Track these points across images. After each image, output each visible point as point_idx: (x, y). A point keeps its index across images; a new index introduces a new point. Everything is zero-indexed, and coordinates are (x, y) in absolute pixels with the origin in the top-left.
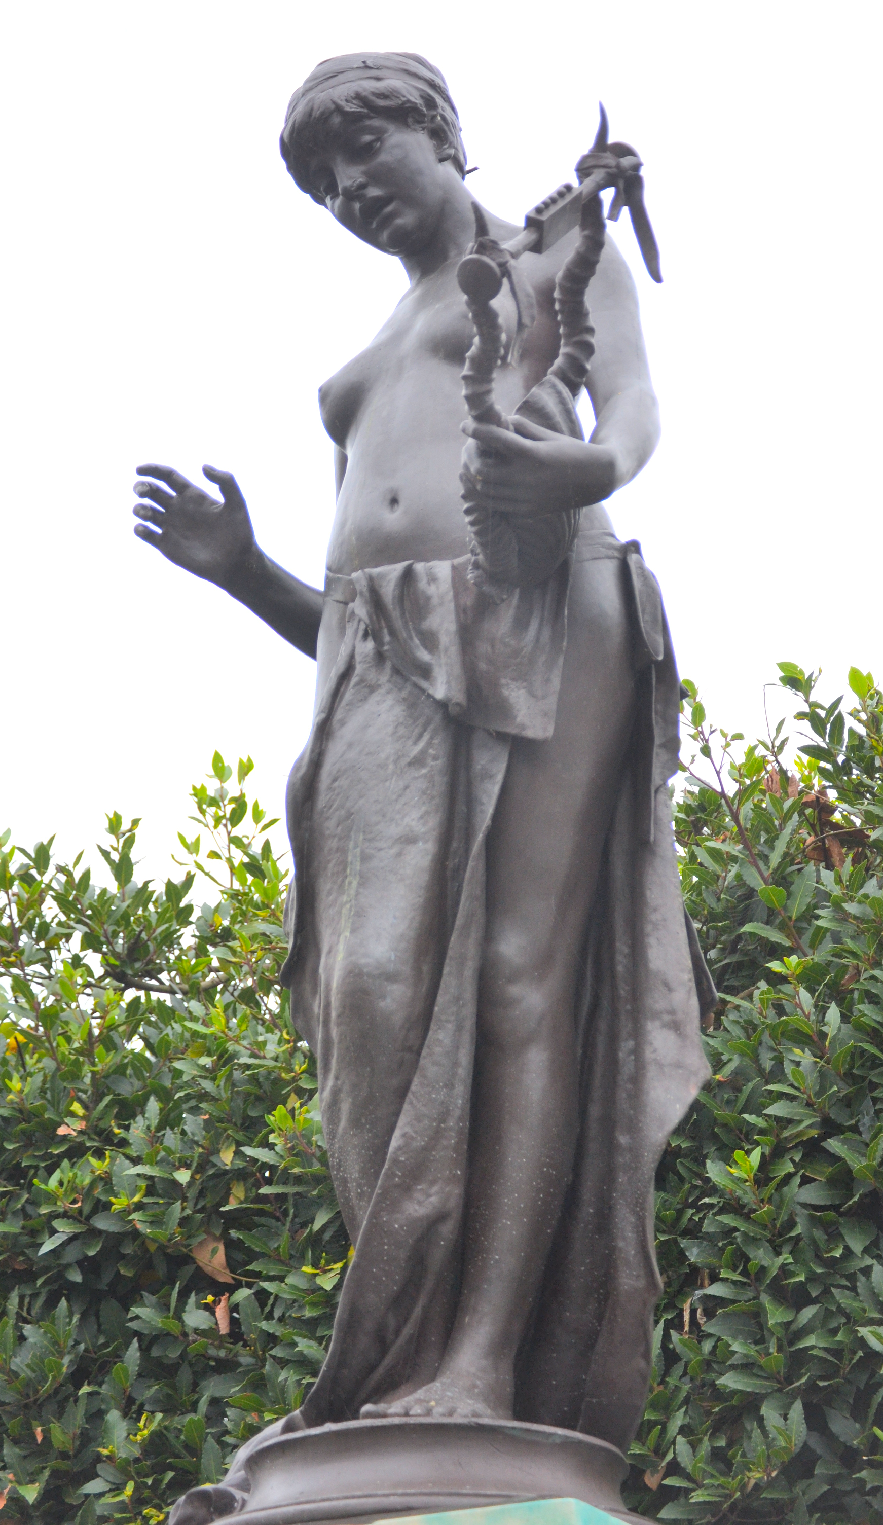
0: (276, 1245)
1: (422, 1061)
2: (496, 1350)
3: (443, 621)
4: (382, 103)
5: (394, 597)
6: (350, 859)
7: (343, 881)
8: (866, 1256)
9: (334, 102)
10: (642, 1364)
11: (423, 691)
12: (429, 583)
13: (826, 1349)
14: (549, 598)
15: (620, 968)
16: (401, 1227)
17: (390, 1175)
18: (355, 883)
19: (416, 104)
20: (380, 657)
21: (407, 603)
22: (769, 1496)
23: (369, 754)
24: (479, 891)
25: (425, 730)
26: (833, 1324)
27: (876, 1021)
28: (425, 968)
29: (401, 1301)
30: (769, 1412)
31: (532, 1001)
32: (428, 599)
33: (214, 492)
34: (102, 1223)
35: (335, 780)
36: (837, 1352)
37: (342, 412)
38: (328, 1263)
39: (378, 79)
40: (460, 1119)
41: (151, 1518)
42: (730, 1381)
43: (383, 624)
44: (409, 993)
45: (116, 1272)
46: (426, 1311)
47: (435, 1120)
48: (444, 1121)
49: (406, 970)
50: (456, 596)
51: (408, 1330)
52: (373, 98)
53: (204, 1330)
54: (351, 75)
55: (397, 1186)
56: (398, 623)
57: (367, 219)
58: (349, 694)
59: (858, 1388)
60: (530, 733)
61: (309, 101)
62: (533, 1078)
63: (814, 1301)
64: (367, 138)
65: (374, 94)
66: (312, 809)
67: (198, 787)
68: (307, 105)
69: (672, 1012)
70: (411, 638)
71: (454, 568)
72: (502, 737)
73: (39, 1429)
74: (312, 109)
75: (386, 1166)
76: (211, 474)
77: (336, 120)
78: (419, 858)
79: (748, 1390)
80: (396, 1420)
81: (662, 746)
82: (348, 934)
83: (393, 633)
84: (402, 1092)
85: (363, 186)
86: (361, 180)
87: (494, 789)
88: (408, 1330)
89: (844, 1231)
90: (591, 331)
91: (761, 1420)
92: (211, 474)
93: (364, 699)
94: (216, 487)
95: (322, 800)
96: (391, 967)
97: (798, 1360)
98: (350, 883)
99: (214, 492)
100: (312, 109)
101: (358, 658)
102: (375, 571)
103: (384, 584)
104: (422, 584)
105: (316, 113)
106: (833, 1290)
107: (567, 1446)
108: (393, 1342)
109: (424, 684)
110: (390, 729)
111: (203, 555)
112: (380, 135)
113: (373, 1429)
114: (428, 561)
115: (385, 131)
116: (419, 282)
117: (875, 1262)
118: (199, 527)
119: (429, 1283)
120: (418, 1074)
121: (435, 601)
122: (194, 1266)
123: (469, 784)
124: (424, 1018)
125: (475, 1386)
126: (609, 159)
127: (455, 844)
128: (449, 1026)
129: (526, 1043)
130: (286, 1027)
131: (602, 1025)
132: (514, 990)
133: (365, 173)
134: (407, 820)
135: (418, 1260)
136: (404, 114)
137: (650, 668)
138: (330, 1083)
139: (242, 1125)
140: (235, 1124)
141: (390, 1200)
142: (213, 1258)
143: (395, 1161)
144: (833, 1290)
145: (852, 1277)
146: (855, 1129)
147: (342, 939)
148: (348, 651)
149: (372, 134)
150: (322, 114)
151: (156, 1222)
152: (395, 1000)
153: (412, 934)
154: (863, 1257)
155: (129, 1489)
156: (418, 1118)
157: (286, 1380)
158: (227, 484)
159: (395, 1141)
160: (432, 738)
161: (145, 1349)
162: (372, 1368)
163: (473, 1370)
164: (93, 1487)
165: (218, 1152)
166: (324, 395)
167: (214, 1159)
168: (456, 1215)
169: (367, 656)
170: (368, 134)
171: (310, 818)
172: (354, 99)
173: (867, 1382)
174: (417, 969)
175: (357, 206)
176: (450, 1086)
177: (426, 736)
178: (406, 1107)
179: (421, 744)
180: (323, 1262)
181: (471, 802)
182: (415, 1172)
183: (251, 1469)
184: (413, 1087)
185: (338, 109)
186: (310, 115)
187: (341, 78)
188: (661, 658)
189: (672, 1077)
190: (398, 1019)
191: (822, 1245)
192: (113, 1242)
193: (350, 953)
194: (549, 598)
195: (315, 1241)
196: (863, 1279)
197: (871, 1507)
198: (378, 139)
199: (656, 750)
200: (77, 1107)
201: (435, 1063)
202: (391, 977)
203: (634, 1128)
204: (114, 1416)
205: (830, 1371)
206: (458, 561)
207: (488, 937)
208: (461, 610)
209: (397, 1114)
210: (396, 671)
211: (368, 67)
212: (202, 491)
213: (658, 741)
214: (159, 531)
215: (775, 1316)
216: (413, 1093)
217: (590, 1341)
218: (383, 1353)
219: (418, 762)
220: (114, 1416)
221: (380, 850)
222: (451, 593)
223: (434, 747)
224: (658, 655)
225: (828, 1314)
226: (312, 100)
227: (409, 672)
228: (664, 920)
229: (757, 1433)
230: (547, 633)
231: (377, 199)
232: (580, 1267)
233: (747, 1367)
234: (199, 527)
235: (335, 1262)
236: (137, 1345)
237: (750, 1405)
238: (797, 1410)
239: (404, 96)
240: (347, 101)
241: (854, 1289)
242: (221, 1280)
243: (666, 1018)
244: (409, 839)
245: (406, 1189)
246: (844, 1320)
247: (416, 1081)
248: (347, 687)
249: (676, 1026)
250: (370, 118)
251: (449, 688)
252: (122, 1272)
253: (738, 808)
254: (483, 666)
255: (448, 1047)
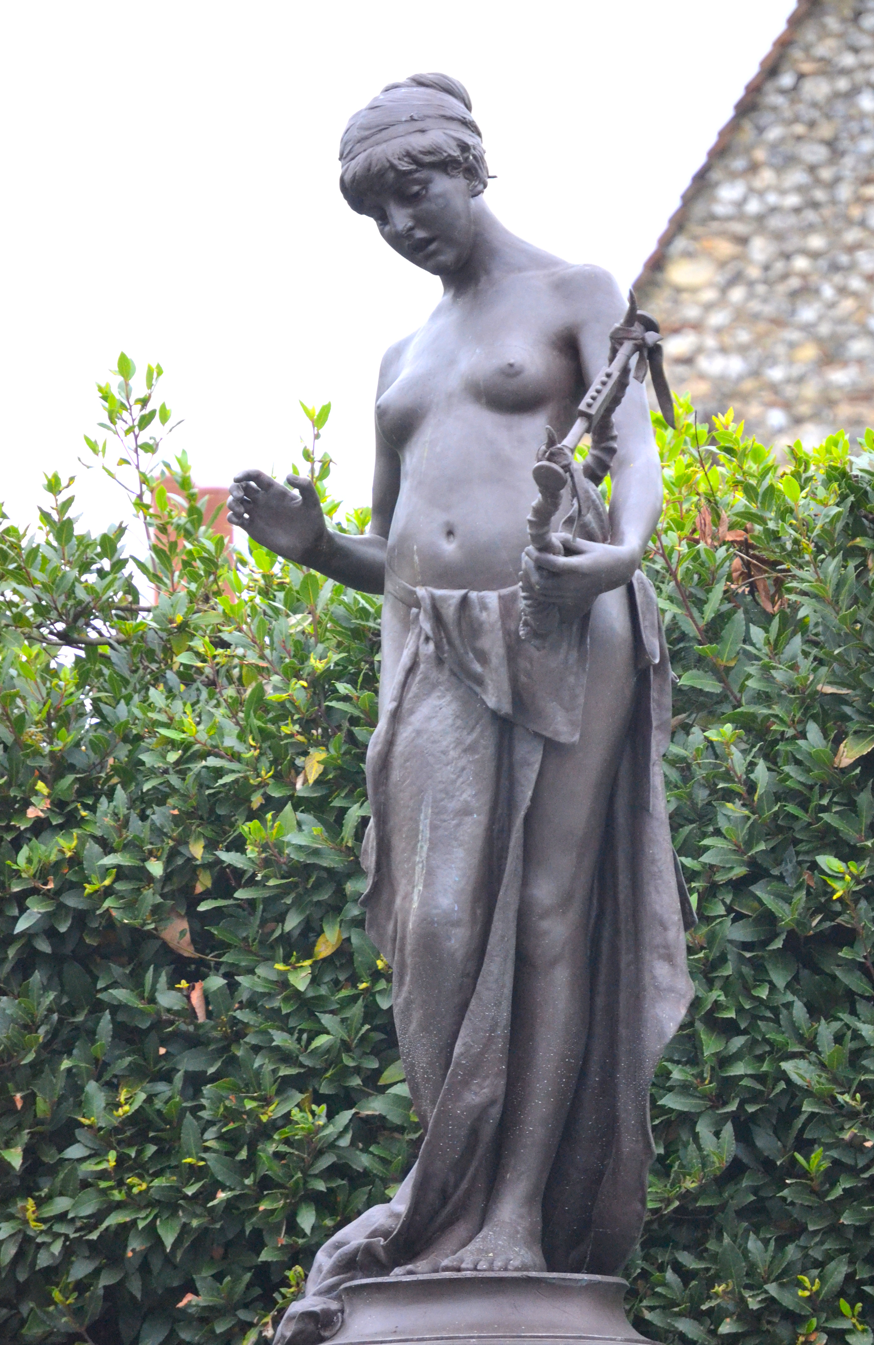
0: (244, 935)
1: (478, 988)
2: (529, 1200)
3: (494, 644)
4: (428, 159)
6: (421, 828)
7: (416, 845)
8: (788, 993)
9: (389, 161)
10: (639, 1206)
11: (477, 694)
12: (481, 611)
13: (751, 1076)
14: (575, 628)
15: (622, 897)
16: (462, 1113)
17: (455, 1074)
21: (464, 624)
22: (704, 1205)
23: (434, 742)
24: (519, 852)
25: (477, 723)
26: (758, 1052)
27: (800, 782)
28: (479, 912)
29: (460, 1168)
30: (703, 1129)
31: (557, 932)
32: (481, 624)
34: (71, 901)
35: (406, 761)
36: (760, 1078)
38: (298, 961)
39: (423, 131)
40: (505, 1028)
41: (133, 1186)
42: (670, 1101)
43: (443, 635)
45: (87, 948)
46: (477, 1170)
47: (486, 1032)
48: (494, 1031)
49: (466, 917)
52: (421, 156)
53: (178, 1011)
54: (401, 129)
56: (457, 642)
58: (414, 689)
59: (780, 1110)
60: (563, 739)
61: (367, 157)
62: (558, 994)
63: (744, 1032)
64: (416, 188)
65: (421, 152)
66: (387, 778)
67: (103, 385)
68: (366, 160)
69: (667, 947)
71: (501, 598)
72: (537, 735)
73: (18, 1096)
74: (370, 164)
75: (451, 1068)
77: (391, 175)
78: (473, 828)
79: (686, 1110)
80: (468, 1274)
81: (658, 727)
82: (421, 888)
86: (410, 224)
87: (532, 774)
88: (464, 1185)
89: (769, 967)
90: (614, 438)
91: (696, 1137)
93: (428, 694)
95: (396, 775)
96: (455, 916)
97: (728, 1085)
98: (422, 847)
100: (370, 164)
101: (422, 658)
103: (445, 606)
105: (375, 169)
106: (759, 1023)
107: (591, 1287)
108: (452, 1194)
109: (478, 689)
110: (450, 721)
111: (284, 540)
112: (426, 183)
113: (451, 1281)
114: (480, 591)
116: (456, 296)
117: (795, 998)
119: (480, 1151)
120: (475, 996)
121: (487, 627)
122: (160, 942)
123: (511, 767)
124: (479, 952)
126: (637, 329)
127: (500, 811)
128: (498, 959)
129: (553, 963)
130: (251, 732)
131: (606, 934)
132: (545, 924)
133: (414, 217)
134: (465, 796)
135: (474, 1133)
136: (446, 165)
137: (648, 668)
138: (404, 994)
139: (208, 818)
140: (201, 818)
142: (177, 932)
143: (458, 1064)
144: (759, 1023)
145: (775, 1010)
146: (781, 878)
147: (416, 891)
148: (413, 649)
150: (380, 170)
151: (130, 906)
152: (457, 941)
153: (469, 888)
154: (785, 994)
155: (112, 1156)
156: (475, 1031)
157: (261, 1066)
159: (458, 1049)
160: (482, 731)
161: (113, 1014)
162: (437, 1213)
163: (514, 1217)
164: (74, 1152)
165: (187, 843)
167: (182, 849)
169: (429, 657)
173: (789, 1104)
176: (498, 1004)
178: (466, 1022)
179: (474, 735)
180: (293, 959)
182: (473, 1071)
185: (393, 167)
186: (369, 170)
189: (669, 999)
190: (460, 955)
191: (750, 980)
192: (81, 918)
193: (422, 904)
194: (575, 628)
195: (285, 938)
196: (784, 1012)
197: (791, 1216)
200: (41, 786)
201: (488, 989)
202: (456, 924)
203: (637, 1037)
204: (92, 1087)
205: (755, 1096)
206: (505, 591)
207: (525, 882)
215: (711, 1046)
216: (472, 1011)
217: (597, 1177)
220: (92, 1087)
221: (445, 821)
222: (500, 623)
224: (654, 657)
225: (754, 1042)
227: (466, 680)
228: (661, 872)
230: (574, 654)
232: (588, 1121)
233: (685, 1089)
235: (305, 959)
236: (109, 1017)
237: (688, 1120)
238: (728, 1130)
241: (777, 1021)
242: (186, 954)
243: (662, 951)
244: (465, 811)
245: (466, 1083)
246: (768, 1049)
247: (473, 1002)
248: (413, 679)
249: (669, 958)
252: (87, 941)
253: (677, 569)
254: (523, 679)
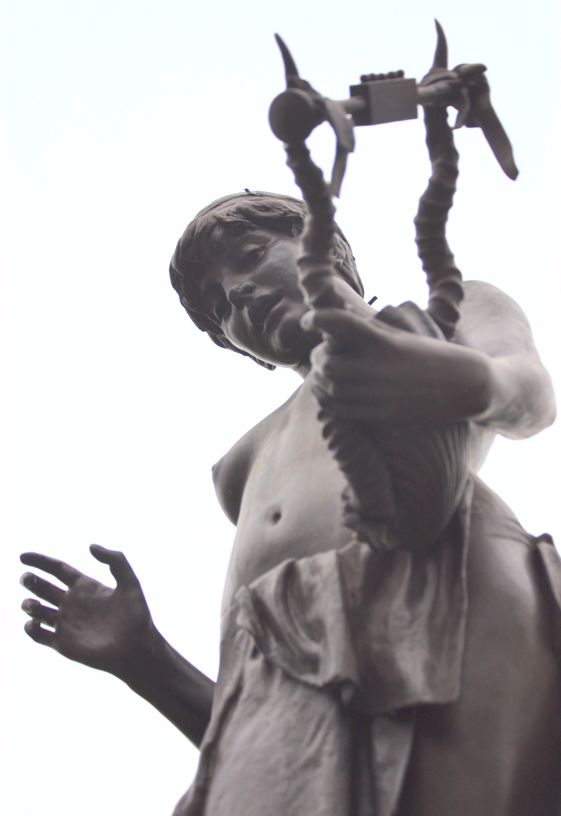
3: (328, 606)
5: (276, 595)
19: (298, 214)
20: (269, 668)
33: (105, 577)
37: (232, 482)
50: (343, 579)
56: (287, 629)
64: (252, 247)
70: (297, 633)
76: (98, 553)
77: (218, 233)
83: (280, 637)
85: (249, 290)
92: (98, 553)
94: (106, 568)
99: (105, 577)
100: (194, 228)
104: (305, 576)
105: (198, 230)
112: (264, 246)
115: (268, 241)
118: (94, 619)
133: (253, 279)
149: (257, 243)
150: (205, 228)
158: (117, 563)
166: (213, 469)
170: (251, 243)
172: (236, 213)
175: (245, 312)
177: (320, 735)
181: (375, 795)
183: (252, 451)
187: (224, 205)
198: (263, 248)
208: (346, 595)
210: (287, 677)
212: (94, 580)
214: (53, 630)
231: (265, 299)
234: (94, 619)
239: (286, 208)
240: (228, 215)
250: (253, 229)
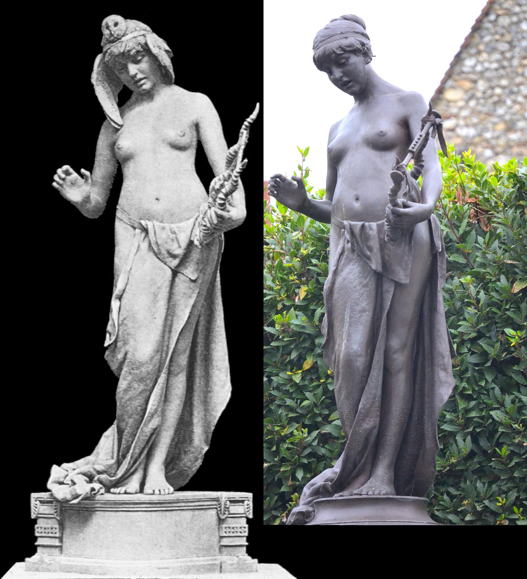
2: (389, 467)
3: (375, 244)
4: (348, 49)
10: (433, 469)
11: (368, 264)
15: (426, 345)
17: (359, 416)
18: (347, 326)
24: (385, 327)
26: (481, 407)
28: (369, 351)
29: (361, 454)
30: (459, 438)
31: (400, 359)
32: (370, 236)
35: (340, 291)
36: (482, 418)
42: (445, 427)
44: (364, 360)
49: (363, 353)
51: (363, 461)
54: (337, 37)
55: (361, 419)
57: (342, 85)
58: (343, 261)
60: (402, 282)
62: (400, 384)
64: (344, 61)
65: (346, 46)
66: (332, 297)
69: (444, 365)
71: (377, 225)
72: (392, 280)
77: (334, 55)
78: (367, 317)
80: (365, 496)
81: (441, 277)
84: (363, 389)
85: (342, 77)
86: (341, 75)
88: (363, 461)
89: (485, 373)
90: (423, 161)
91: (456, 441)
93: (349, 264)
95: (335, 296)
96: (359, 353)
101: (346, 249)
102: (353, 223)
104: (368, 230)
105: (327, 53)
107: (414, 501)
108: (358, 464)
109: (368, 262)
110: (357, 275)
111: (290, 202)
112: (347, 59)
116: (360, 104)
121: (372, 237)
124: (369, 367)
125: (384, 480)
126: (432, 117)
128: (376, 370)
129: (398, 372)
131: (420, 360)
132: (395, 356)
133: (343, 72)
134: (363, 304)
135: (367, 440)
136: (356, 52)
141: (359, 424)
143: (360, 412)
145: (488, 391)
146: (490, 338)
147: (343, 343)
148: (342, 246)
152: (360, 363)
153: (365, 342)
156: (367, 399)
157: (281, 413)
168: (378, 427)
171: (332, 300)
173: (493, 428)
174: (367, 355)
176: (377, 388)
178: (363, 395)
179: (367, 280)
180: (294, 370)
182: (367, 414)
184: (366, 389)
185: (334, 52)
188: (440, 250)
189: (445, 386)
190: (361, 368)
191: (478, 379)
193: (347, 348)
195: (291, 362)
196: (491, 391)
199: (439, 279)
201: (372, 382)
202: (360, 356)
203: (432, 401)
205: (479, 425)
206: (379, 222)
207: (387, 339)
209: (361, 396)
211: (342, 33)
213: (439, 276)
215: (462, 405)
218: (355, 468)
219: (365, 286)
223: (371, 282)
225: (479, 403)
226: (325, 48)
229: (454, 445)
230: (407, 248)
232: (413, 435)
233: (451, 422)
235: (299, 370)
237: (453, 434)
238: (469, 438)
241: (488, 395)
243: (442, 367)
244: (363, 311)
245: (363, 420)
246: (485, 406)
251: (377, 266)
254: (386, 257)
255: (376, 374)
